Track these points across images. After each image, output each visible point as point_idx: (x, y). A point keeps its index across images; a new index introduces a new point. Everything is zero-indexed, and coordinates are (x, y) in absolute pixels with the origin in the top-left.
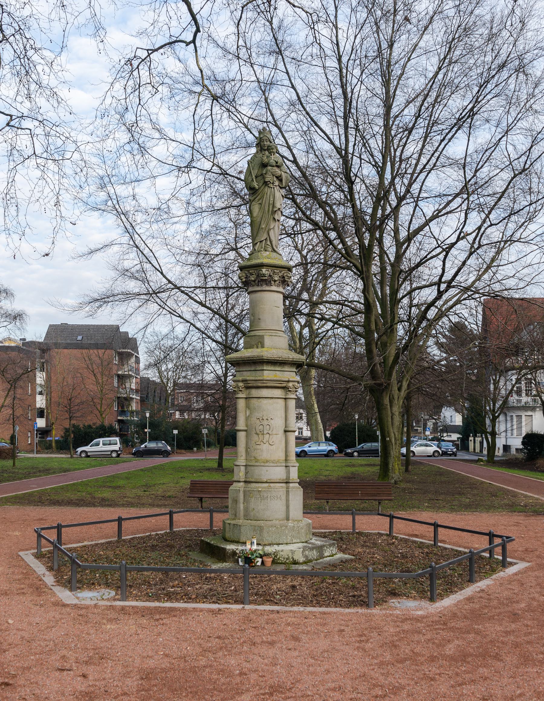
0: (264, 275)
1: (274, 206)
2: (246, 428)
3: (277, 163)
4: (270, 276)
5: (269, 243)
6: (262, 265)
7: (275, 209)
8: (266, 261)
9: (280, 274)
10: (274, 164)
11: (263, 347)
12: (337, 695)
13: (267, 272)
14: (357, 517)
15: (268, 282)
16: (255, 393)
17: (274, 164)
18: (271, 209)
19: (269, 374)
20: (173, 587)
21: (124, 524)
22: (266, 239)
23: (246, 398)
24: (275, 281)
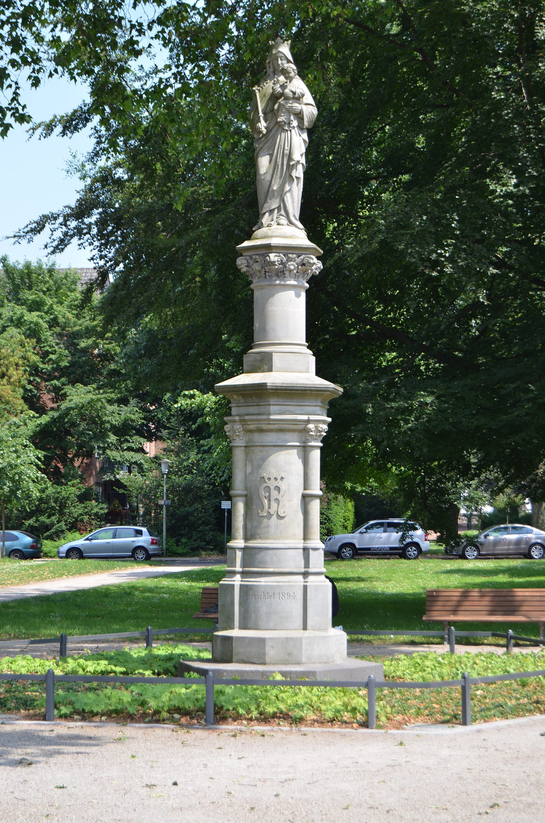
0: (273, 263)
1: (290, 158)
2: (245, 492)
3: (294, 93)
4: (282, 263)
5: (282, 212)
6: (269, 248)
7: (292, 163)
8: (274, 241)
9: (298, 260)
10: (291, 95)
11: (270, 370)
12: (444, 816)
13: (276, 259)
14: (301, 551)
15: (281, 273)
16: (257, 438)
17: (291, 95)
18: (285, 162)
19: (279, 413)
20: (33, 691)
21: (453, 708)
22: (279, 208)
23: (246, 447)
24: (290, 271)
